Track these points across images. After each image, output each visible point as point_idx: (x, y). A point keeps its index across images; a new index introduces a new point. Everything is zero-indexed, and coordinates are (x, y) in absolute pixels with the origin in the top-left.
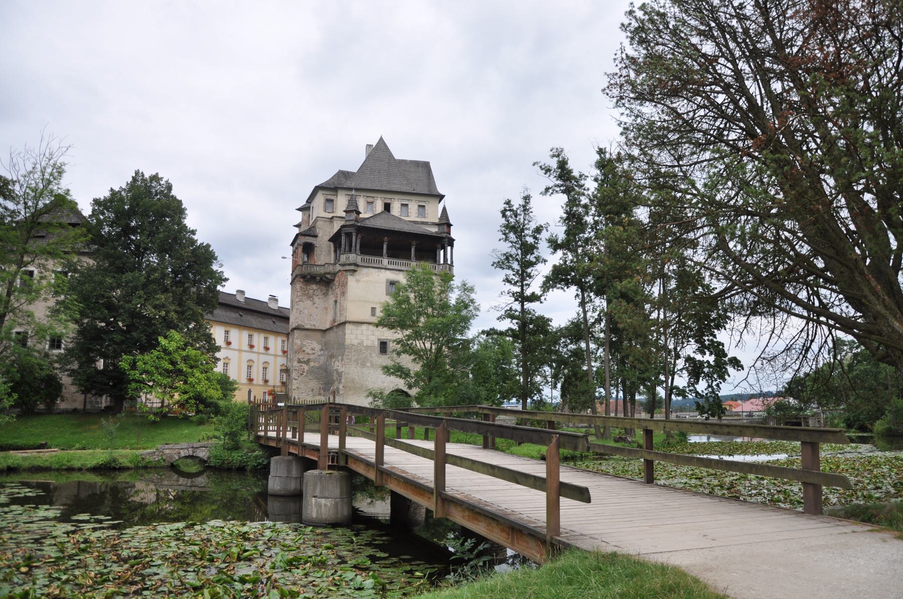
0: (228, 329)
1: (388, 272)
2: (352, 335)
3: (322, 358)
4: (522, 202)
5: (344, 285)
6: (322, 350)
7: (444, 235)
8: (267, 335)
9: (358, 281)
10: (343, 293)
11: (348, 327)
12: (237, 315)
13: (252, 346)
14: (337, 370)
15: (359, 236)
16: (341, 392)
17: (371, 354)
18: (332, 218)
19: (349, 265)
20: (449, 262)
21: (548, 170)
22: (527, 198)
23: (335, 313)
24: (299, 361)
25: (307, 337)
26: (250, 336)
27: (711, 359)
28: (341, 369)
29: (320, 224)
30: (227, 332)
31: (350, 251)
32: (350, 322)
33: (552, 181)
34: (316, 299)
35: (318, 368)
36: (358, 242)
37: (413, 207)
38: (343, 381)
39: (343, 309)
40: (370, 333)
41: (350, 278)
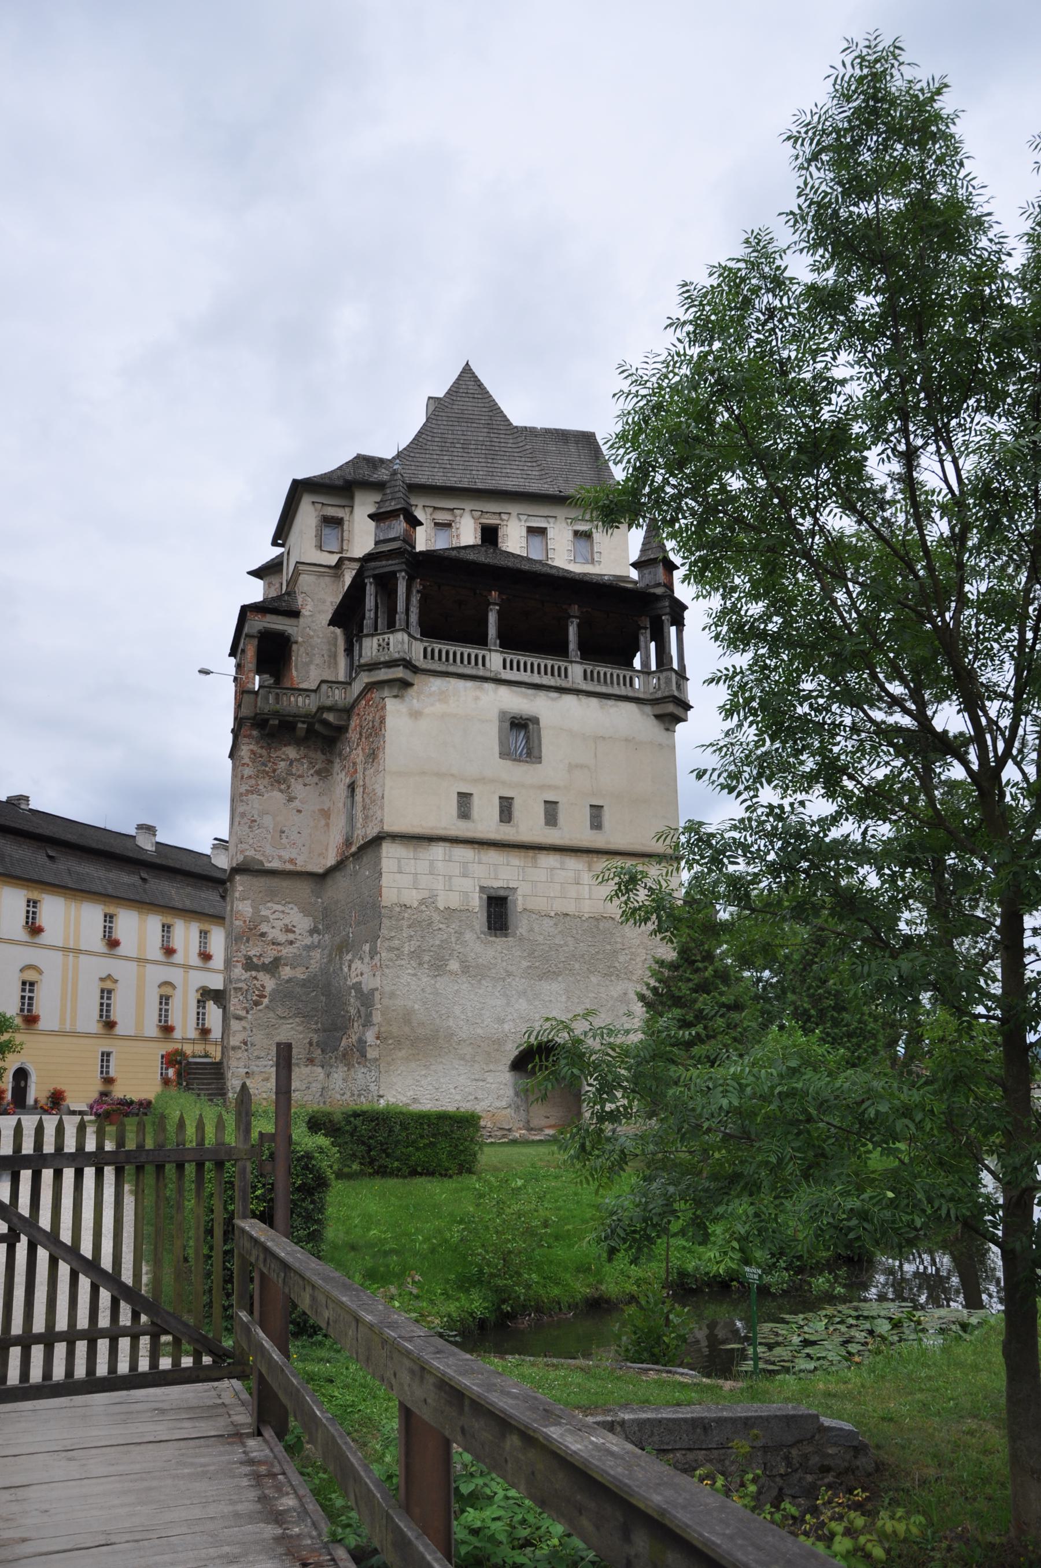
0: (111, 910)
1: (503, 691)
2: (400, 876)
3: (317, 954)
5: (377, 729)
6: (314, 931)
7: (659, 591)
8: (206, 927)
9: (416, 715)
10: (373, 755)
11: (390, 852)
12: (135, 879)
13: (169, 951)
14: (357, 987)
15: (417, 585)
16: (371, 1054)
17: (459, 934)
20: (675, 666)
23: (351, 819)
24: (249, 965)
25: (272, 895)
26: (167, 928)
28: (369, 983)
29: (306, 581)
30: (109, 918)
31: (391, 626)
32: (395, 837)
34: (297, 788)
35: (304, 984)
36: (415, 599)
38: (377, 1018)
39: (375, 800)
40: (456, 869)
41: (392, 706)
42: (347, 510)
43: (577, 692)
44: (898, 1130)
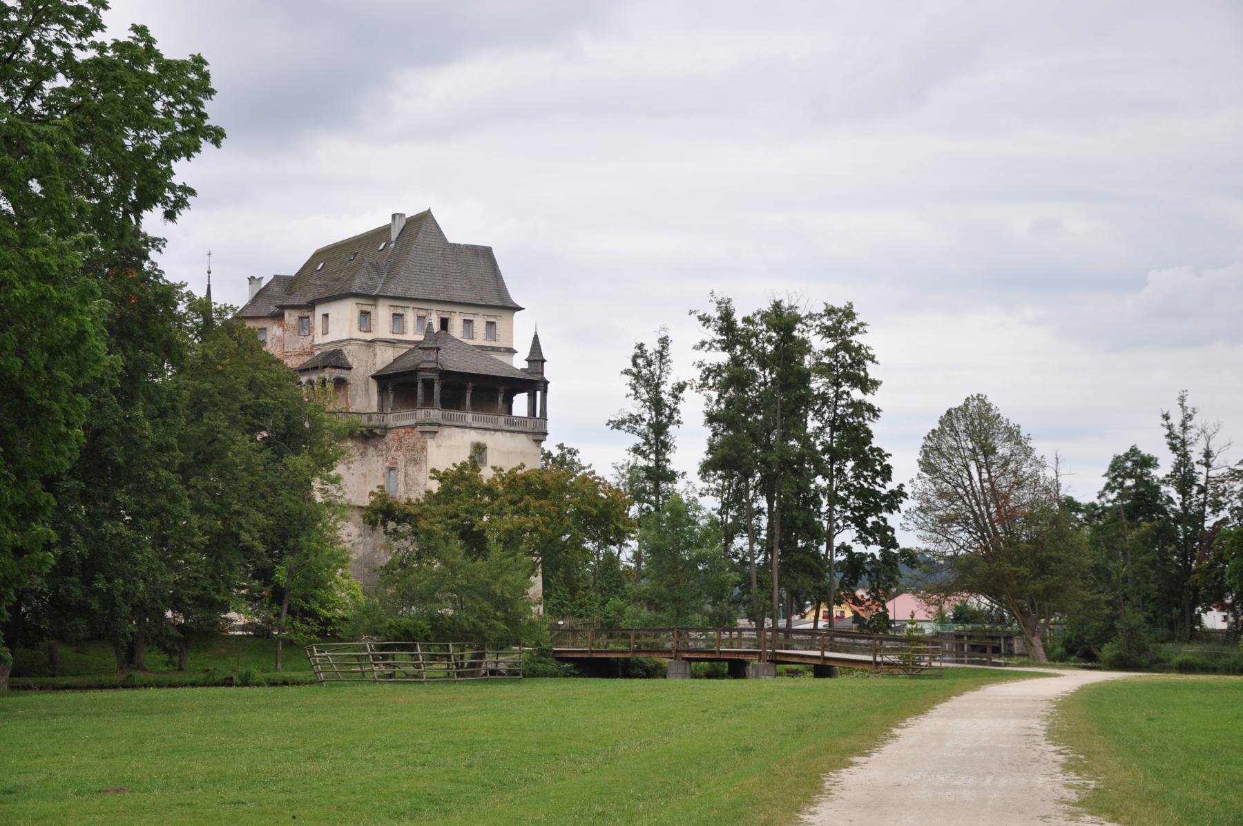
1: (473, 432)
3: (361, 547)
4: (658, 348)
6: (360, 535)
9: (439, 446)
19: (430, 424)
21: (705, 320)
22: (664, 342)
27: (875, 550)
33: (711, 334)
37: (480, 324)
43: (501, 430)
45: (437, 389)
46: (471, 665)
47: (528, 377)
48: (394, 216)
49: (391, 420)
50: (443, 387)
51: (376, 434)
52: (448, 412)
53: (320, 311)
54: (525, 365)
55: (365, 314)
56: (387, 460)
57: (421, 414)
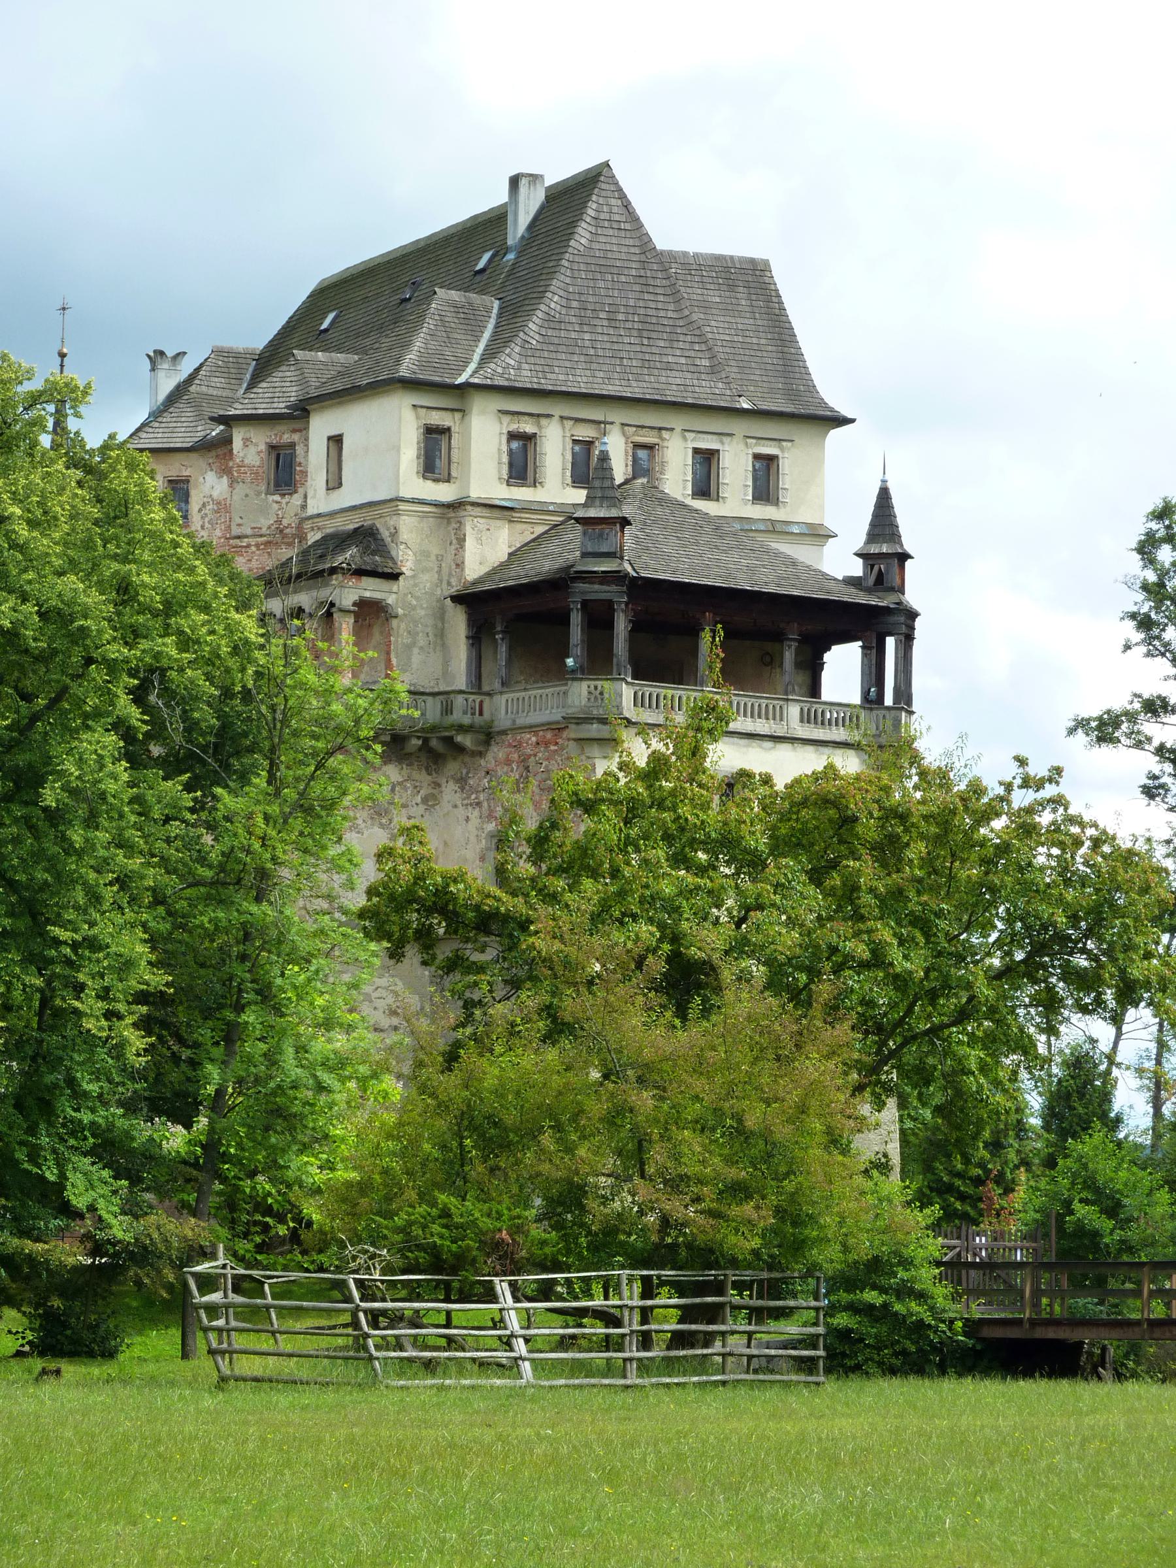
18: (456, 506)
37: (736, 467)
42: (458, 415)
44: (129, 1237)
45: (621, 625)
46: (679, 1340)
47: (862, 599)
48: (514, 182)
49: (503, 708)
50: (637, 628)
51: (460, 749)
52: (651, 689)
53: (321, 426)
54: (857, 568)
55: (434, 436)
56: (490, 816)
57: (580, 693)
